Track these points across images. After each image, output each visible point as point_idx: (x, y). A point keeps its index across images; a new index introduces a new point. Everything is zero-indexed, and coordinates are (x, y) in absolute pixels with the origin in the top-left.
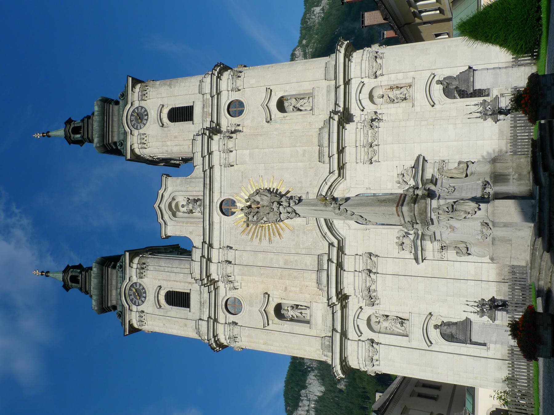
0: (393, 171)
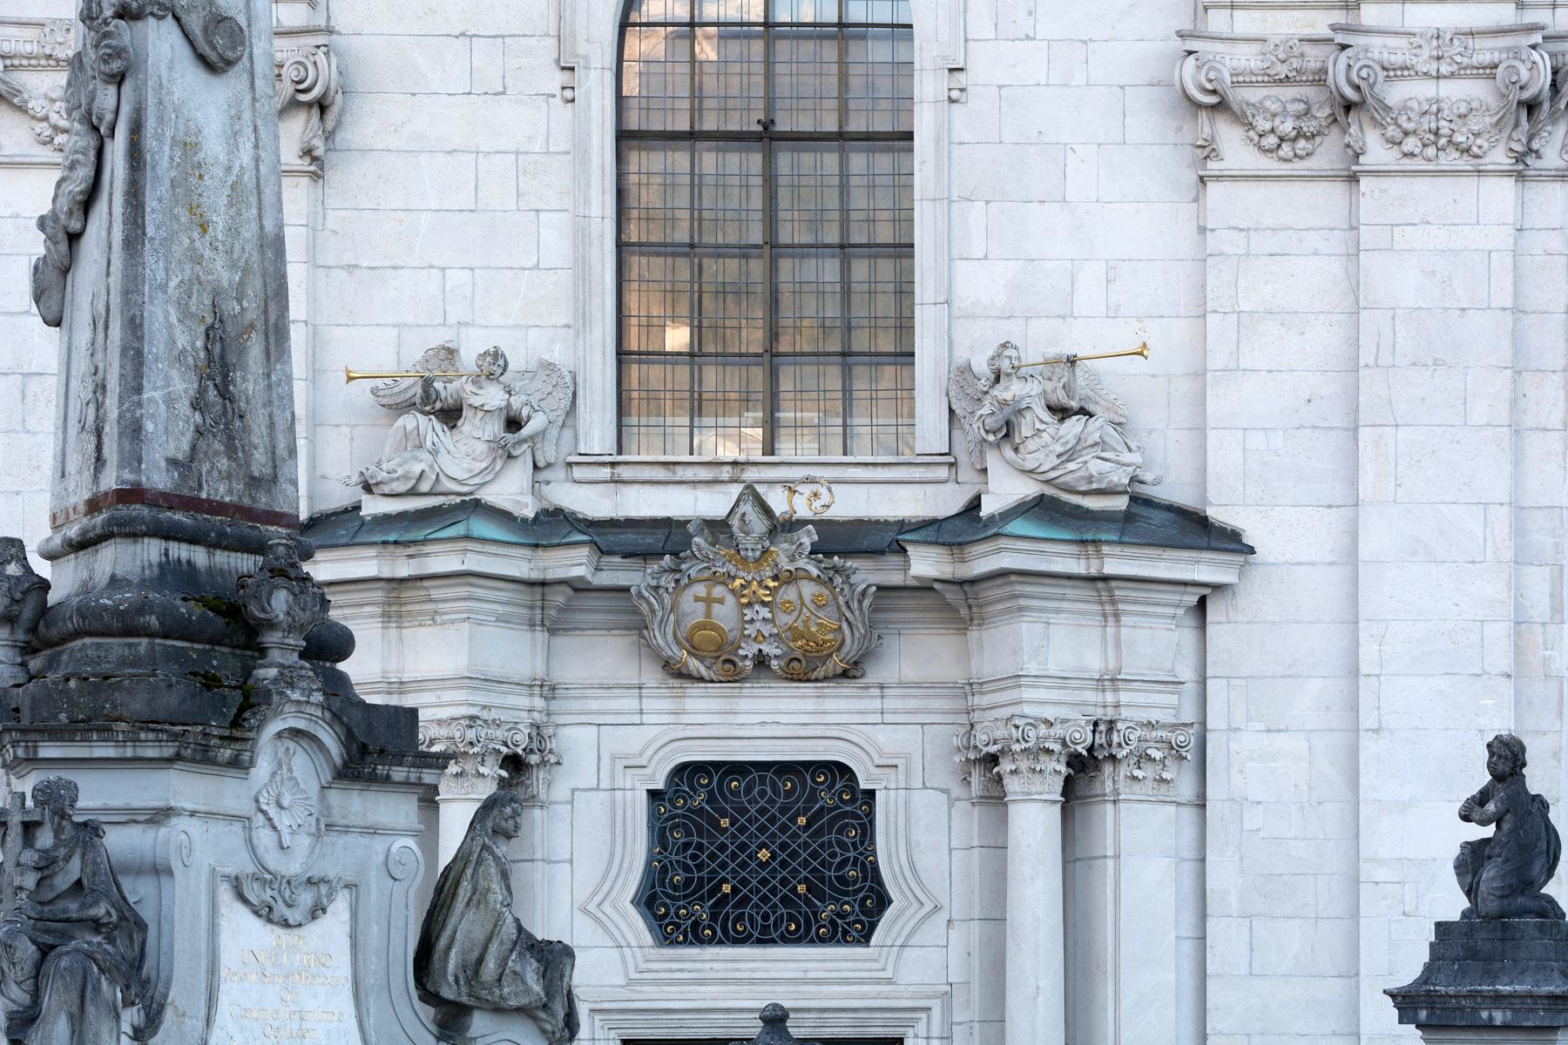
0: (1113, 313)
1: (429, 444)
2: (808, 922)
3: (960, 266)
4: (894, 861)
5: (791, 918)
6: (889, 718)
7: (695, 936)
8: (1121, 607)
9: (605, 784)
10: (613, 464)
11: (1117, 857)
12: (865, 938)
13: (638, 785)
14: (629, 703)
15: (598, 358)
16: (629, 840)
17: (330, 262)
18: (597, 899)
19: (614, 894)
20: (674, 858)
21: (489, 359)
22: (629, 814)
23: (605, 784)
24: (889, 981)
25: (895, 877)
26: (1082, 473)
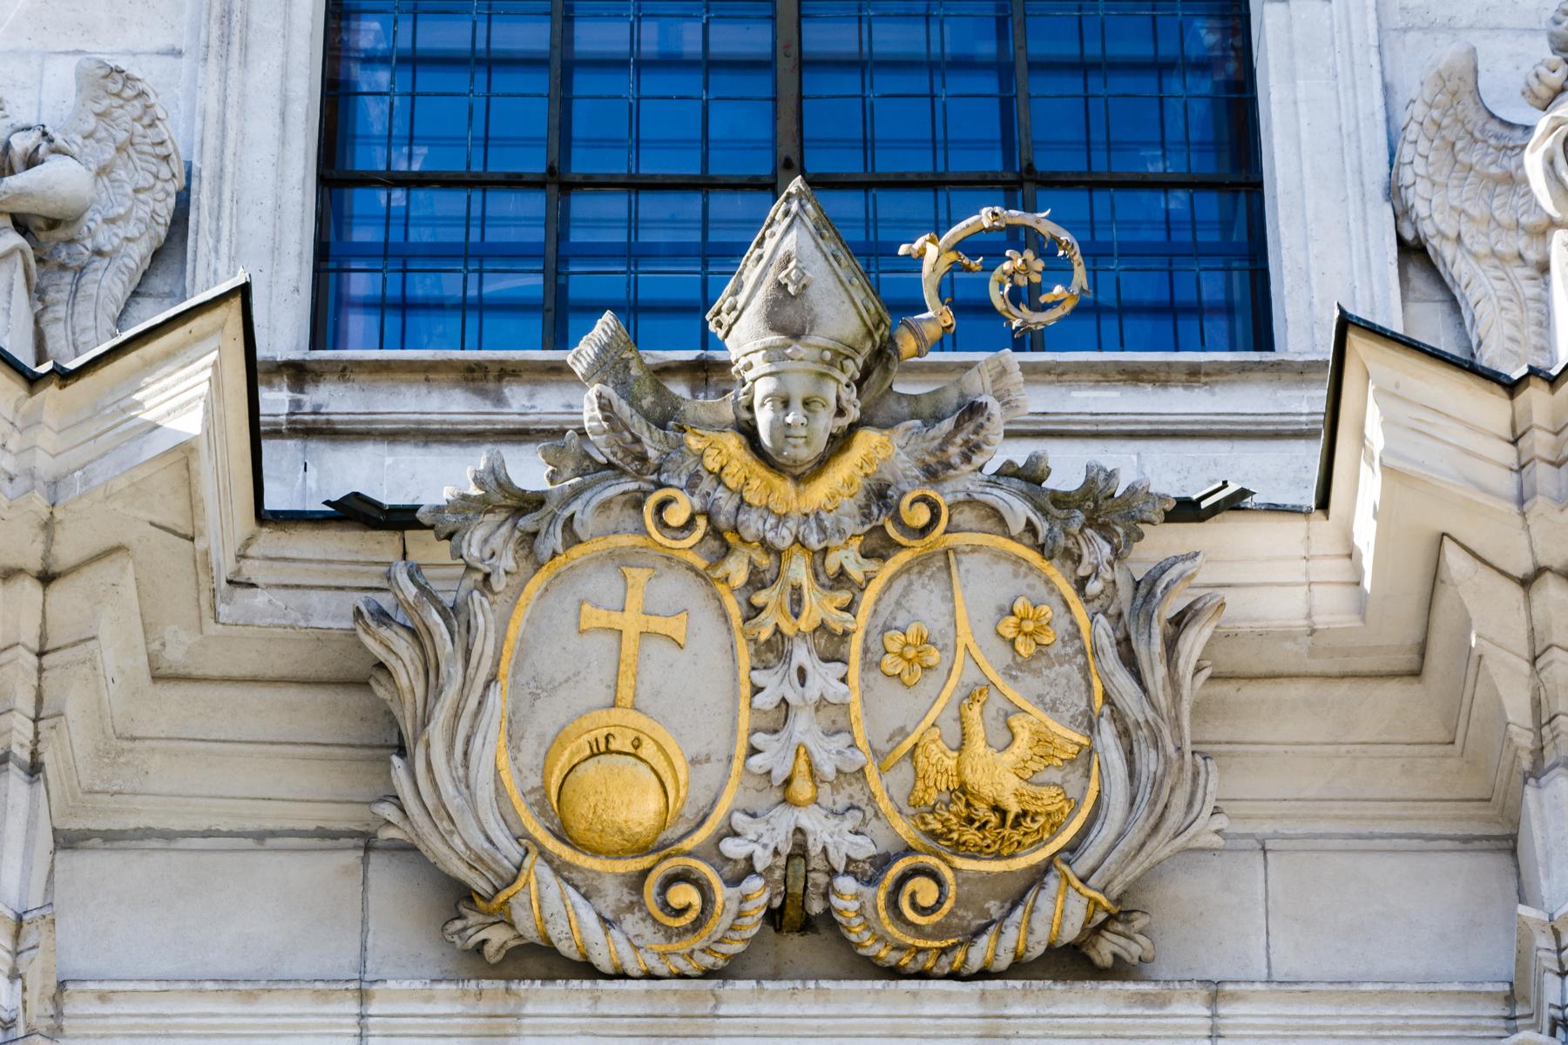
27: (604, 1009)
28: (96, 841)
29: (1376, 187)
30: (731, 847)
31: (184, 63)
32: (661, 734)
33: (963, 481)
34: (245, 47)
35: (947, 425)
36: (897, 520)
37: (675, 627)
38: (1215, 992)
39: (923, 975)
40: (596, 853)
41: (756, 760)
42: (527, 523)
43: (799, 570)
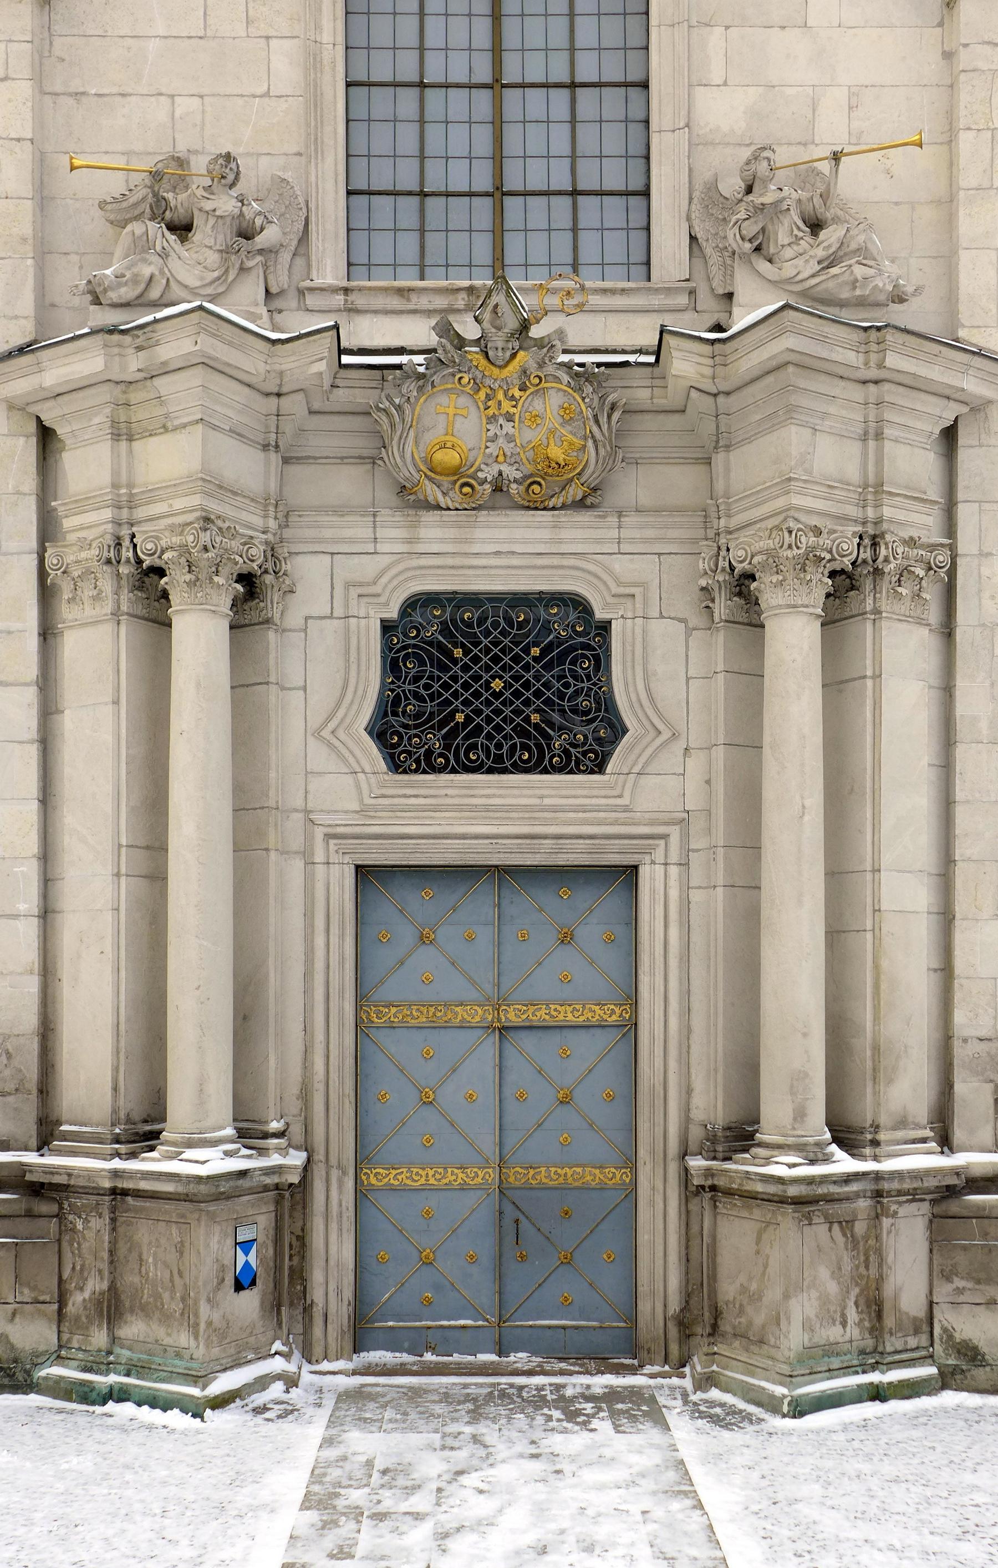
1: (158, 248)
2: (539, 746)
3: (699, 92)
4: (631, 689)
5: (525, 747)
6: (625, 548)
7: (428, 765)
8: (888, 415)
9: (339, 612)
10: (346, 291)
11: (877, 676)
12: (599, 767)
13: (372, 613)
14: (359, 529)
15: (330, 185)
16: (363, 668)
17: (58, 88)
18: (331, 726)
19: (348, 721)
20: (407, 687)
21: (221, 161)
22: (363, 642)
23: (339, 612)
24: (626, 809)
25: (632, 706)
26: (846, 277)
27: (444, 519)
28: (294, 460)
29: (684, 215)
30: (480, 475)
31: (303, 158)
32: (460, 442)
33: (550, 369)
34: (322, 156)
35: (545, 350)
36: (530, 381)
37: (464, 412)
38: (620, 514)
39: (536, 509)
40: (441, 475)
41: (487, 450)
42: (421, 383)
43: (500, 396)
